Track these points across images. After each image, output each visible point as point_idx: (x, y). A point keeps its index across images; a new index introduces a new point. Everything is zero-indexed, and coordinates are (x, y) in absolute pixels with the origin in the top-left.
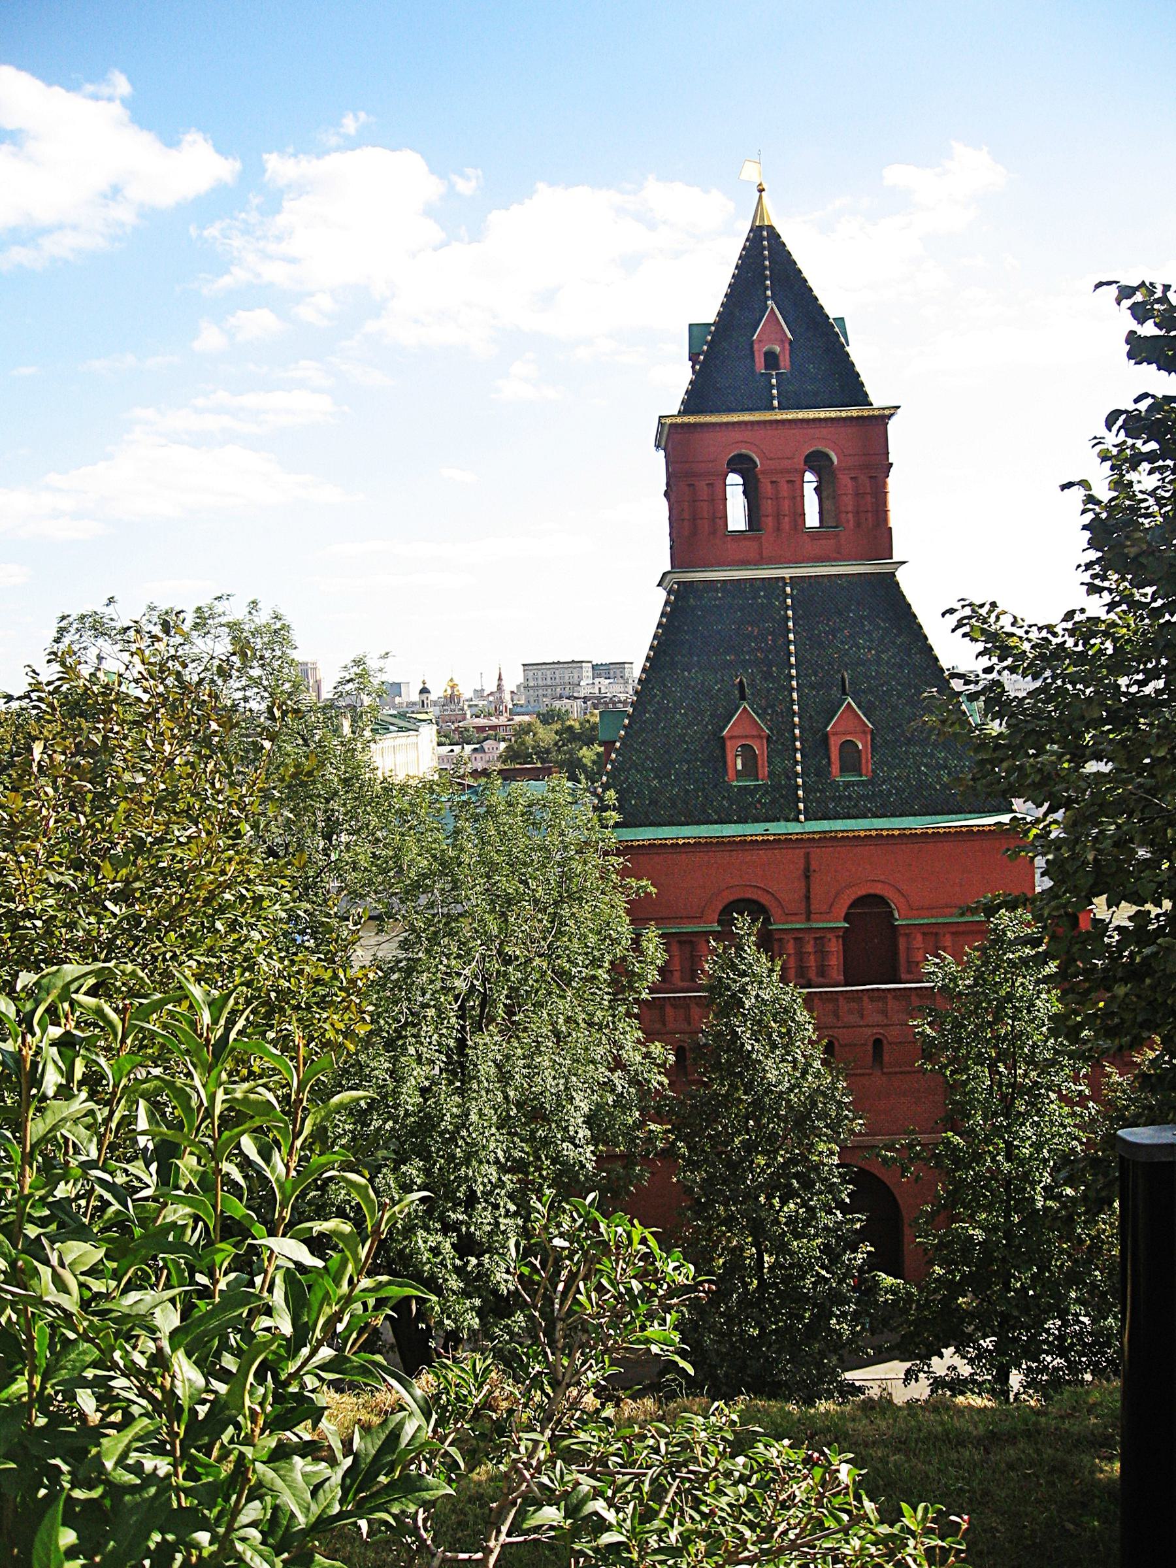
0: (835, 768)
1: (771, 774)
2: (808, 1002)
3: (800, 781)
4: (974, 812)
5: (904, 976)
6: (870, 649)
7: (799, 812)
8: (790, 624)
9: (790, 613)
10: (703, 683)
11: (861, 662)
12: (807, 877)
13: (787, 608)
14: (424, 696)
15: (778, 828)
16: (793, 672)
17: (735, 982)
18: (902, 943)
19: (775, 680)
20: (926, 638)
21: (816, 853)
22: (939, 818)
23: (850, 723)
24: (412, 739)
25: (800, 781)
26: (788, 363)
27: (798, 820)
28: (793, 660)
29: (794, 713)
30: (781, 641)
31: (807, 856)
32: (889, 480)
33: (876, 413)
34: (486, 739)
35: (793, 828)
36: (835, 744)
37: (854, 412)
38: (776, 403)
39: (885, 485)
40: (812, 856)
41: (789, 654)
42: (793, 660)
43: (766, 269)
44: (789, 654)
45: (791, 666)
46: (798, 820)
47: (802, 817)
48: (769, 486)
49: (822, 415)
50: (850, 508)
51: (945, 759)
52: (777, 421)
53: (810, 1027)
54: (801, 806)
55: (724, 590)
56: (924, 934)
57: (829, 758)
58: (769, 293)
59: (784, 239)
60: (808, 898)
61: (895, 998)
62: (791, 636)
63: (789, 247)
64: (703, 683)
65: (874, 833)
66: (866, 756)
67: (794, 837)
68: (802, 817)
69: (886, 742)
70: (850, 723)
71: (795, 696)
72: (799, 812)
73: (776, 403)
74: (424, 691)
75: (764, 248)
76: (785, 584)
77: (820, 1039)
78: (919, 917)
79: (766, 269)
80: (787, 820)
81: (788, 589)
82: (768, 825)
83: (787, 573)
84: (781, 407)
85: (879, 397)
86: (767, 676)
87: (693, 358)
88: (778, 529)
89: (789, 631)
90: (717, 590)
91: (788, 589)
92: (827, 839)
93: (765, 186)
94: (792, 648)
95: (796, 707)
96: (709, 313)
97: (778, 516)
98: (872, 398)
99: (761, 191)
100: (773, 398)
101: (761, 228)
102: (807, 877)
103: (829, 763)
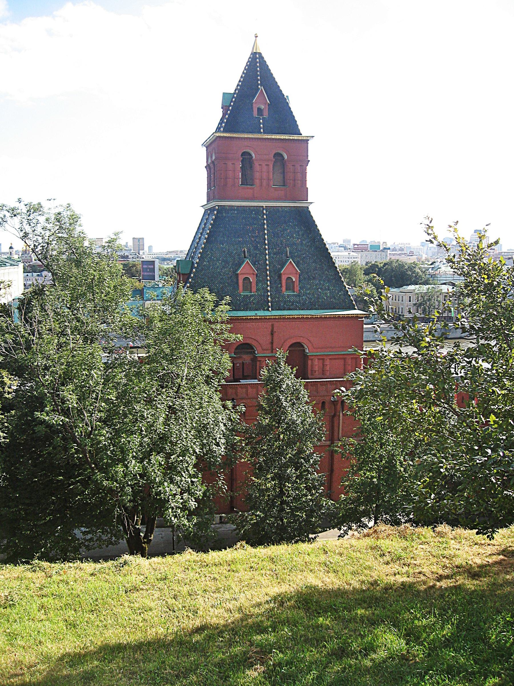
0: (284, 289)
1: (258, 290)
2: (306, 386)
3: (269, 293)
4: (340, 309)
5: (310, 376)
6: (298, 239)
7: (269, 307)
8: (266, 226)
9: (265, 221)
10: (229, 249)
11: (294, 244)
12: (272, 334)
13: (264, 219)
14: (11, 250)
15: (261, 313)
16: (267, 247)
17: (278, 377)
18: (310, 362)
19: (259, 250)
20: (321, 235)
21: (276, 324)
22: (326, 311)
23: (291, 270)
24: (16, 270)
25: (269, 293)
26: (267, 114)
27: (268, 310)
28: (266, 242)
29: (267, 264)
30: (261, 233)
31: (273, 326)
32: (307, 167)
33: (305, 138)
34: (43, 270)
35: (267, 313)
36: (284, 278)
37: (296, 137)
38: (262, 130)
39: (306, 169)
40: (275, 326)
41: (265, 239)
42: (266, 242)
43: (257, 75)
44: (265, 239)
45: (266, 244)
46: (268, 310)
47: (270, 309)
48: (258, 166)
49: (282, 137)
50: (291, 178)
51: (328, 286)
52: (263, 139)
53: (307, 396)
54: (270, 304)
55: (237, 210)
56: (318, 359)
57: (281, 284)
58: (259, 82)
59: (265, 59)
60: (272, 343)
61: (311, 385)
62: (266, 231)
63: (268, 63)
64: (229, 249)
65: (300, 317)
66: (297, 284)
67: (268, 317)
68: (270, 309)
69: (305, 278)
70: (291, 270)
71: (267, 257)
72: (269, 307)
73: (262, 130)
74: (11, 248)
75: (257, 62)
76: (264, 209)
77: (311, 401)
78: (317, 352)
79: (257, 75)
80: (264, 310)
81: (265, 211)
82: (256, 312)
83: (264, 204)
84: (264, 133)
85: (305, 130)
86: (256, 248)
87: (224, 108)
88: (261, 185)
89: (265, 229)
90: (234, 210)
91: (265, 211)
92: (282, 318)
93: (258, 35)
94: (266, 236)
95: (268, 262)
96: (231, 89)
97: (261, 179)
98: (301, 132)
99: (256, 37)
100: (261, 128)
101: (256, 53)
102: (272, 334)
103: (281, 287)
